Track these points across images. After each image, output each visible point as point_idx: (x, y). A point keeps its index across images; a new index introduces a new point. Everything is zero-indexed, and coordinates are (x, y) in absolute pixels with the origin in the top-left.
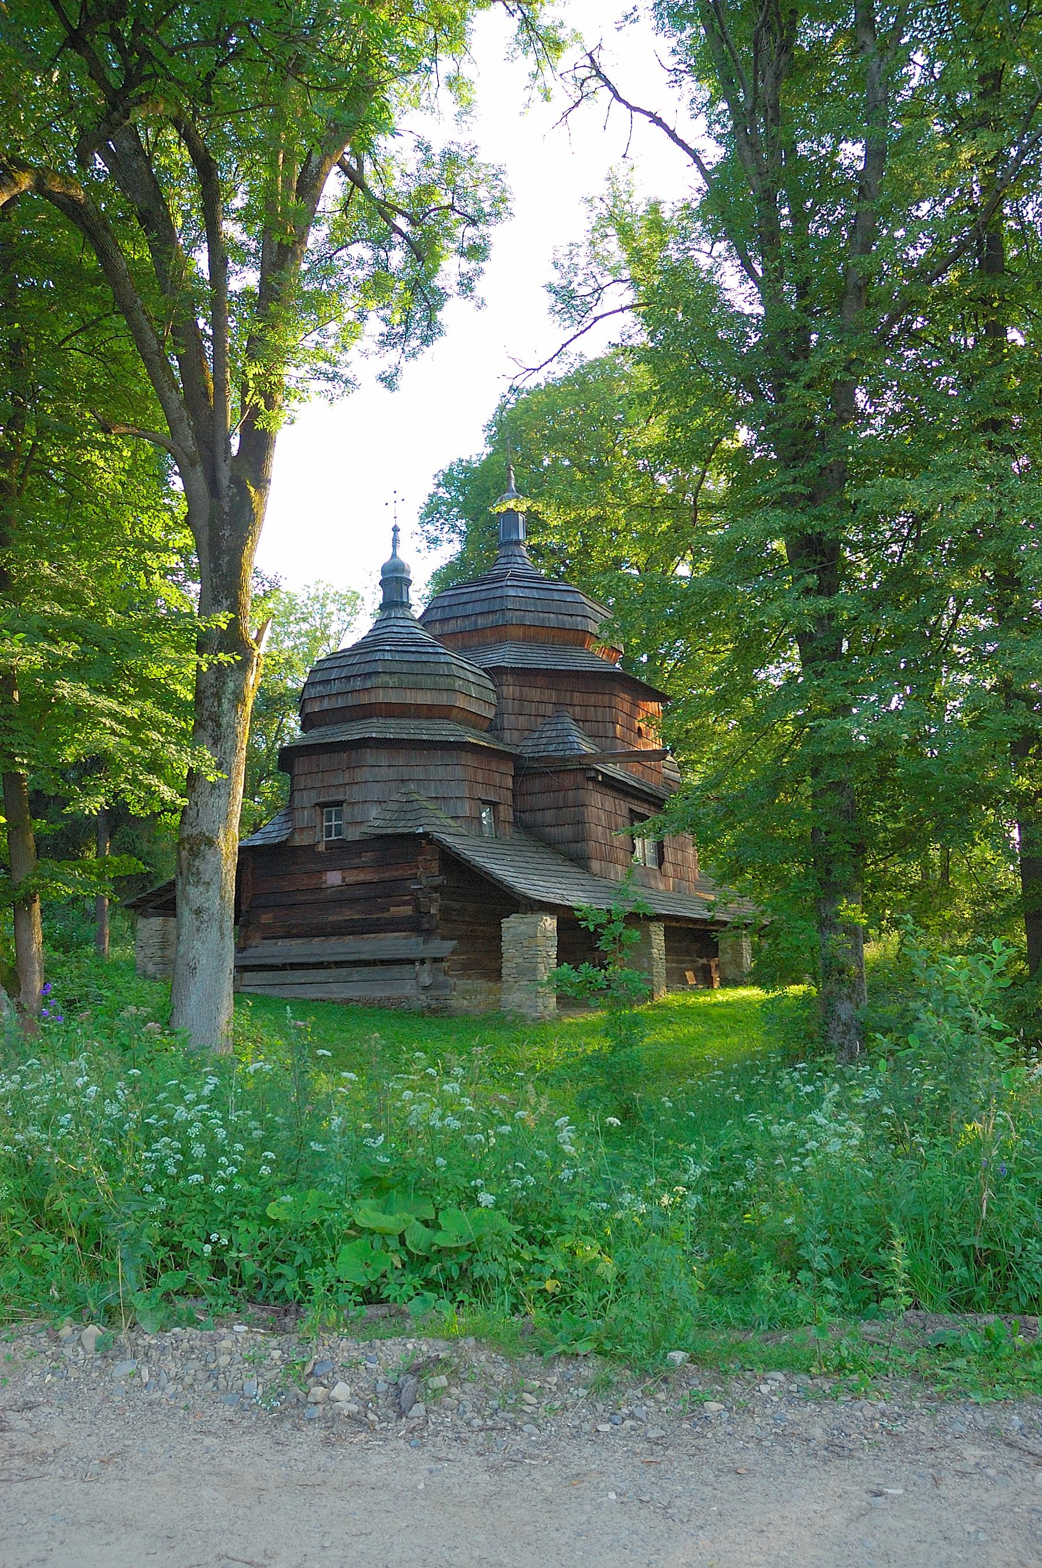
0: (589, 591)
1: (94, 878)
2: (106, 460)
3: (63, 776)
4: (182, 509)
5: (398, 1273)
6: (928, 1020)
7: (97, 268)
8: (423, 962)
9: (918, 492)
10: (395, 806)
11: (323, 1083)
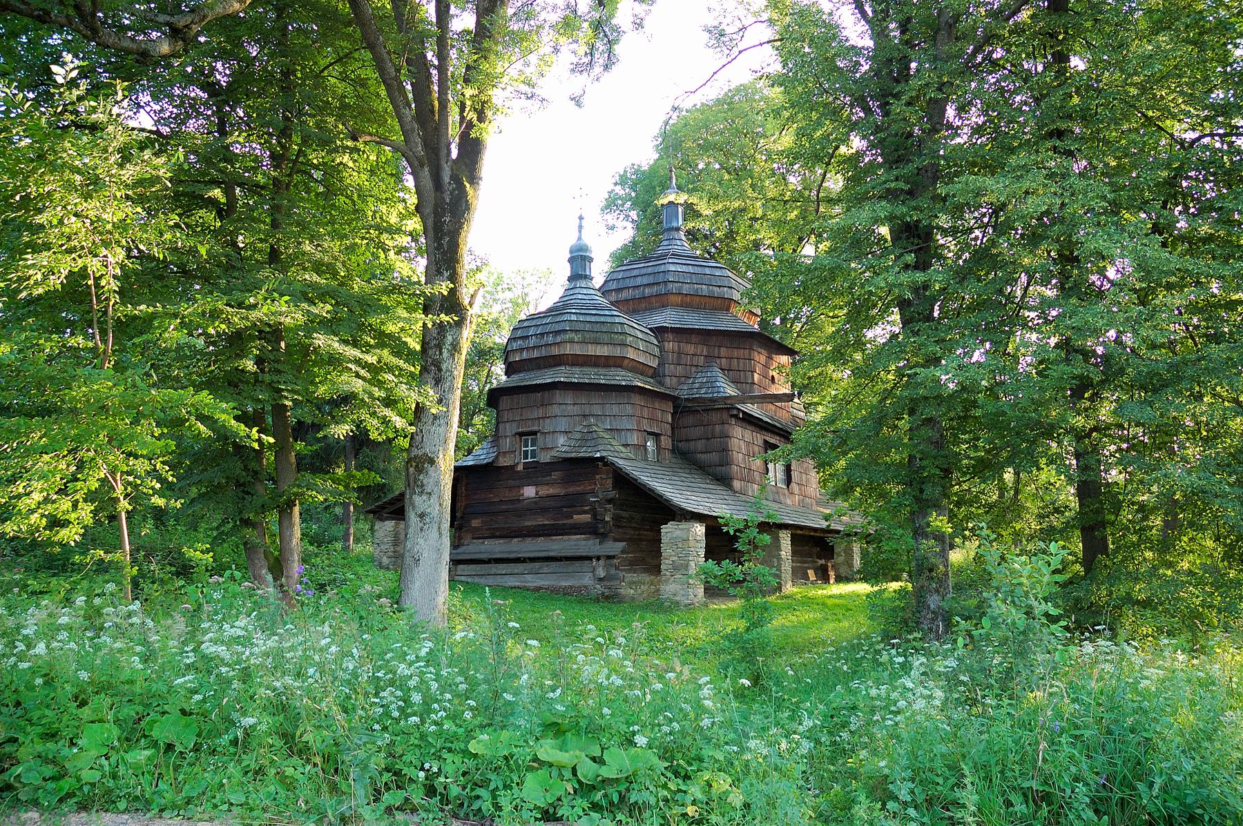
0: (734, 267)
1: (341, 488)
2: (355, 161)
3: (319, 409)
4: (413, 200)
5: (570, 797)
6: (999, 607)
7: (349, 14)
8: (598, 558)
9: (995, 187)
10: (578, 436)
11: (513, 649)
